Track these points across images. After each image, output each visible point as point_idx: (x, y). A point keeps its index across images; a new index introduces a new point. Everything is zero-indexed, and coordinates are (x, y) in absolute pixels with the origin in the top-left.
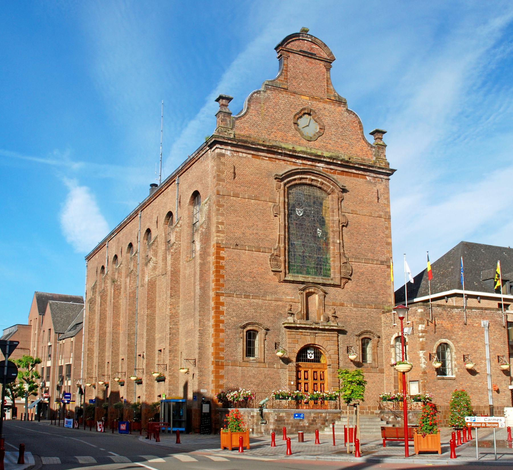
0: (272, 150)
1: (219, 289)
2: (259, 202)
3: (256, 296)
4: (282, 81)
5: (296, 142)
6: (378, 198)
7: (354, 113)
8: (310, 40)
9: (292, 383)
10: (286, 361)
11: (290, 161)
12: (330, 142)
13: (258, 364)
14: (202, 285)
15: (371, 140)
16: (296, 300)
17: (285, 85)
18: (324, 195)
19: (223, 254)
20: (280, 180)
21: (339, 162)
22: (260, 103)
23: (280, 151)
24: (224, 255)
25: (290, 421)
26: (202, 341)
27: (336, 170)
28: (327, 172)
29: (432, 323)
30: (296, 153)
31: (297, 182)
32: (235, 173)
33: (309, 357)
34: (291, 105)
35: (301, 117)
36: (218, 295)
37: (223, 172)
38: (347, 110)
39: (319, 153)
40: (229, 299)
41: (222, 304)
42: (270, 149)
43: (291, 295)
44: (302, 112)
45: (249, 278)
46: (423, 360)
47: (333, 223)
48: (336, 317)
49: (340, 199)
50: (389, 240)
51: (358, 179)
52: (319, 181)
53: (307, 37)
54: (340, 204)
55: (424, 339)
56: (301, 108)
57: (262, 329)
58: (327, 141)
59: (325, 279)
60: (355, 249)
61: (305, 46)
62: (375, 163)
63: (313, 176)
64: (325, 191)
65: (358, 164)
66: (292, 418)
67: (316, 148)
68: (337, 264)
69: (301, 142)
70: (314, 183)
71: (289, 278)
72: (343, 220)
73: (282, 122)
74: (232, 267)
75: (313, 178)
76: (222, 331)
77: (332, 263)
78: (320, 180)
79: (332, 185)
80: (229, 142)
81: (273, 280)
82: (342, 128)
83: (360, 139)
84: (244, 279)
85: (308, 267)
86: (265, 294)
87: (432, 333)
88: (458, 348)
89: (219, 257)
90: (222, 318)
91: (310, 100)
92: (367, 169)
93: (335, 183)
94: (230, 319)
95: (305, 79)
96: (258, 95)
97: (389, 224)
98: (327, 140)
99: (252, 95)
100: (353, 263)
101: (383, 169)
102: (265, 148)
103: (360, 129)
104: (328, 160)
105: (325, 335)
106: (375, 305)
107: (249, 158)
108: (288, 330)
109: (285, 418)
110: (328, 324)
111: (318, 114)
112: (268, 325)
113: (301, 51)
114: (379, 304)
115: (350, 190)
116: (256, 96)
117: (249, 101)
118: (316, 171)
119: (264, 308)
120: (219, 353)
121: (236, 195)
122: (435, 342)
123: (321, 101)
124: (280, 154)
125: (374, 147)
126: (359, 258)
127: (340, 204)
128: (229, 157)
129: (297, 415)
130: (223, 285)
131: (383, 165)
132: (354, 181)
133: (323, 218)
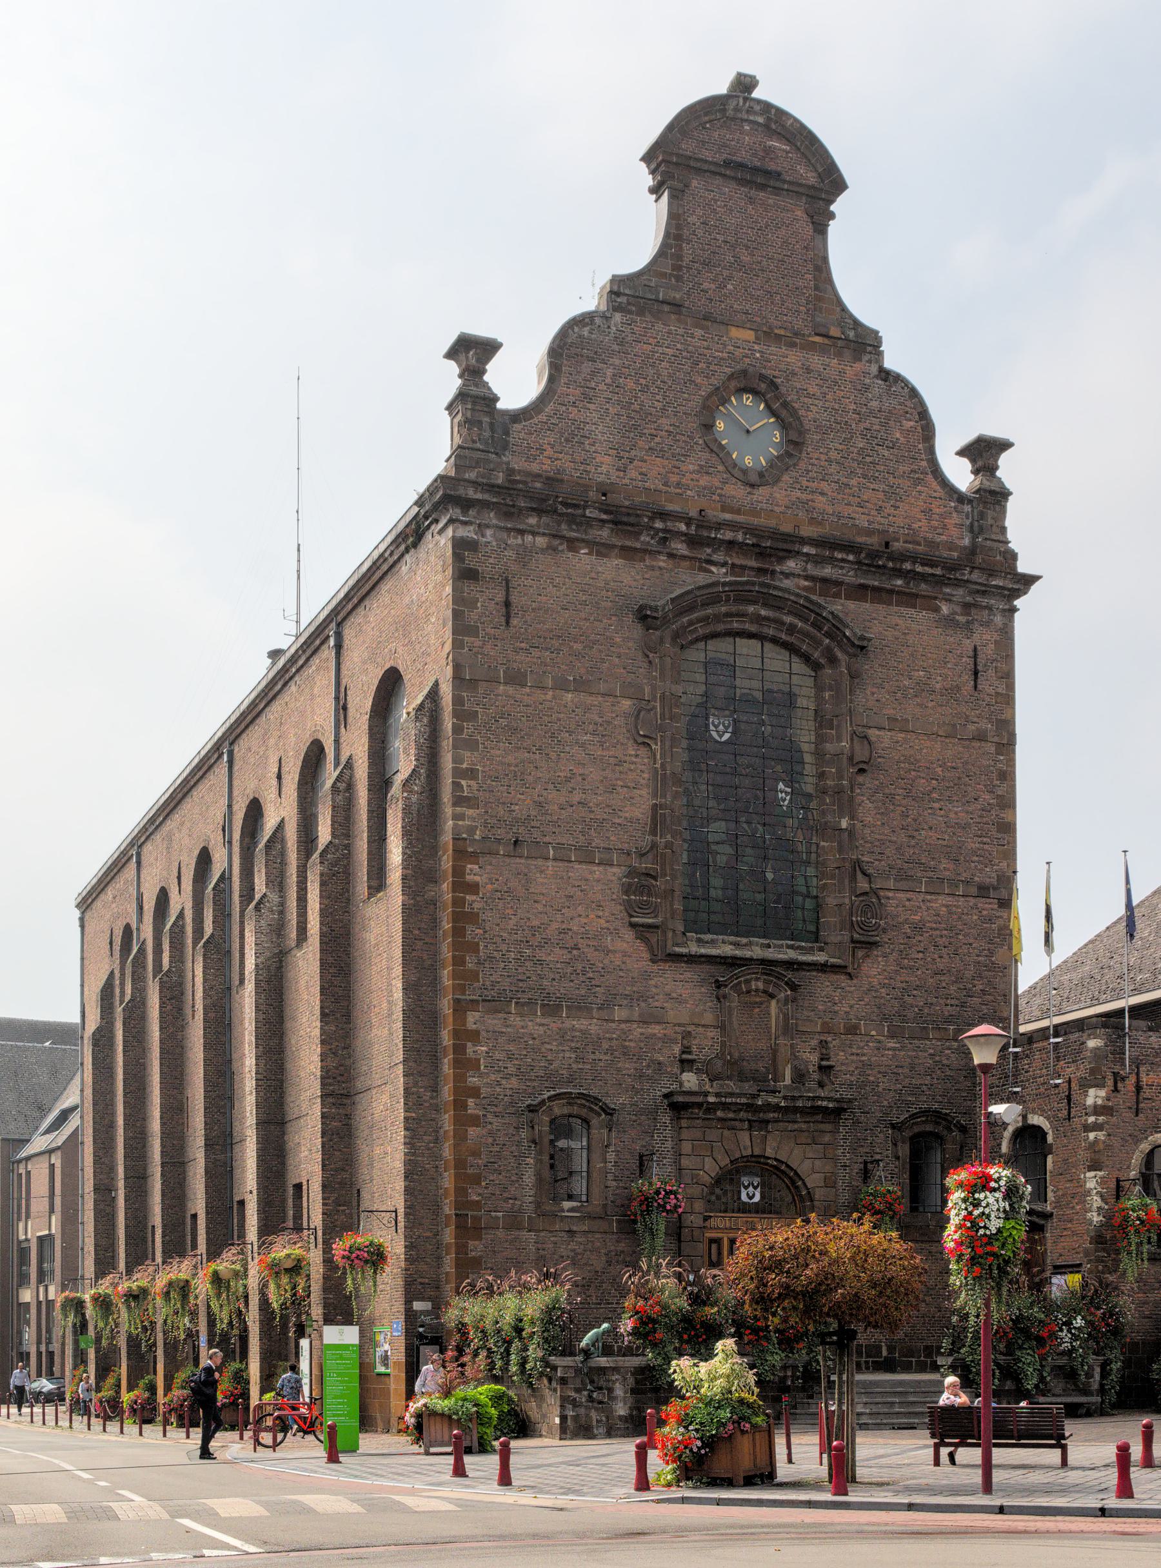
19: (473, 873)
36: (460, 1008)
41: (475, 1036)
46: (1097, 1202)
76: (475, 1121)
81: (628, 951)
86: (606, 1006)
89: (462, 886)
98: (813, 479)
119: (605, 1046)
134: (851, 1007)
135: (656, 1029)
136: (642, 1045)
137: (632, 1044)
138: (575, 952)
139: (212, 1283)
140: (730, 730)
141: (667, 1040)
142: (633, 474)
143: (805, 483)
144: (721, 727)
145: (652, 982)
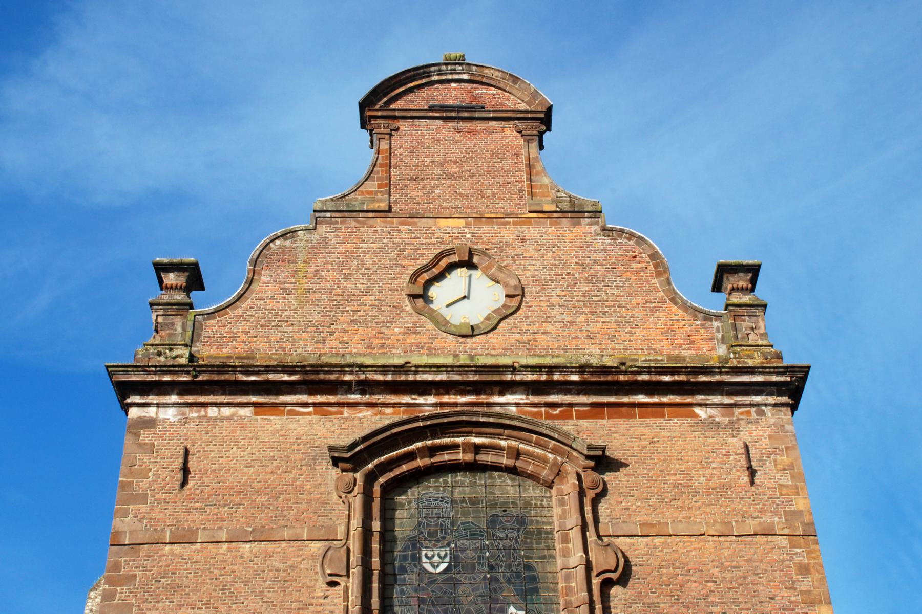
0: (318, 381)
2: (270, 547)
4: (371, 193)
5: (419, 346)
6: (752, 472)
8: (465, 77)
11: (394, 405)
12: (548, 327)
18: (533, 492)
20: (349, 466)
21: (575, 378)
22: (295, 262)
23: (348, 377)
27: (571, 405)
28: (539, 414)
30: (407, 373)
31: (420, 462)
32: (186, 470)
35: (440, 277)
44: (444, 263)
47: (567, 578)
49: (591, 494)
51: (660, 421)
53: (454, 72)
54: (588, 508)
58: (534, 328)
63: (479, 435)
67: (490, 351)
69: (437, 344)
70: (487, 458)
72: (602, 560)
73: (370, 300)
78: (503, 443)
79: (554, 451)
80: (166, 378)
82: (588, 281)
83: (663, 301)
92: (688, 383)
93: (564, 443)
95: (450, 176)
96: (288, 243)
101: (751, 370)
102: (294, 378)
103: (659, 274)
104: (530, 377)
113: (432, 108)
115: (632, 460)
116: (280, 247)
118: (485, 415)
121: (185, 538)
124: (348, 387)
125: (718, 317)
127: (588, 508)
128: (172, 424)
132: (646, 430)
133: (528, 567)
140: (447, 559)
142: (335, 344)
143: (525, 327)
144: (436, 559)
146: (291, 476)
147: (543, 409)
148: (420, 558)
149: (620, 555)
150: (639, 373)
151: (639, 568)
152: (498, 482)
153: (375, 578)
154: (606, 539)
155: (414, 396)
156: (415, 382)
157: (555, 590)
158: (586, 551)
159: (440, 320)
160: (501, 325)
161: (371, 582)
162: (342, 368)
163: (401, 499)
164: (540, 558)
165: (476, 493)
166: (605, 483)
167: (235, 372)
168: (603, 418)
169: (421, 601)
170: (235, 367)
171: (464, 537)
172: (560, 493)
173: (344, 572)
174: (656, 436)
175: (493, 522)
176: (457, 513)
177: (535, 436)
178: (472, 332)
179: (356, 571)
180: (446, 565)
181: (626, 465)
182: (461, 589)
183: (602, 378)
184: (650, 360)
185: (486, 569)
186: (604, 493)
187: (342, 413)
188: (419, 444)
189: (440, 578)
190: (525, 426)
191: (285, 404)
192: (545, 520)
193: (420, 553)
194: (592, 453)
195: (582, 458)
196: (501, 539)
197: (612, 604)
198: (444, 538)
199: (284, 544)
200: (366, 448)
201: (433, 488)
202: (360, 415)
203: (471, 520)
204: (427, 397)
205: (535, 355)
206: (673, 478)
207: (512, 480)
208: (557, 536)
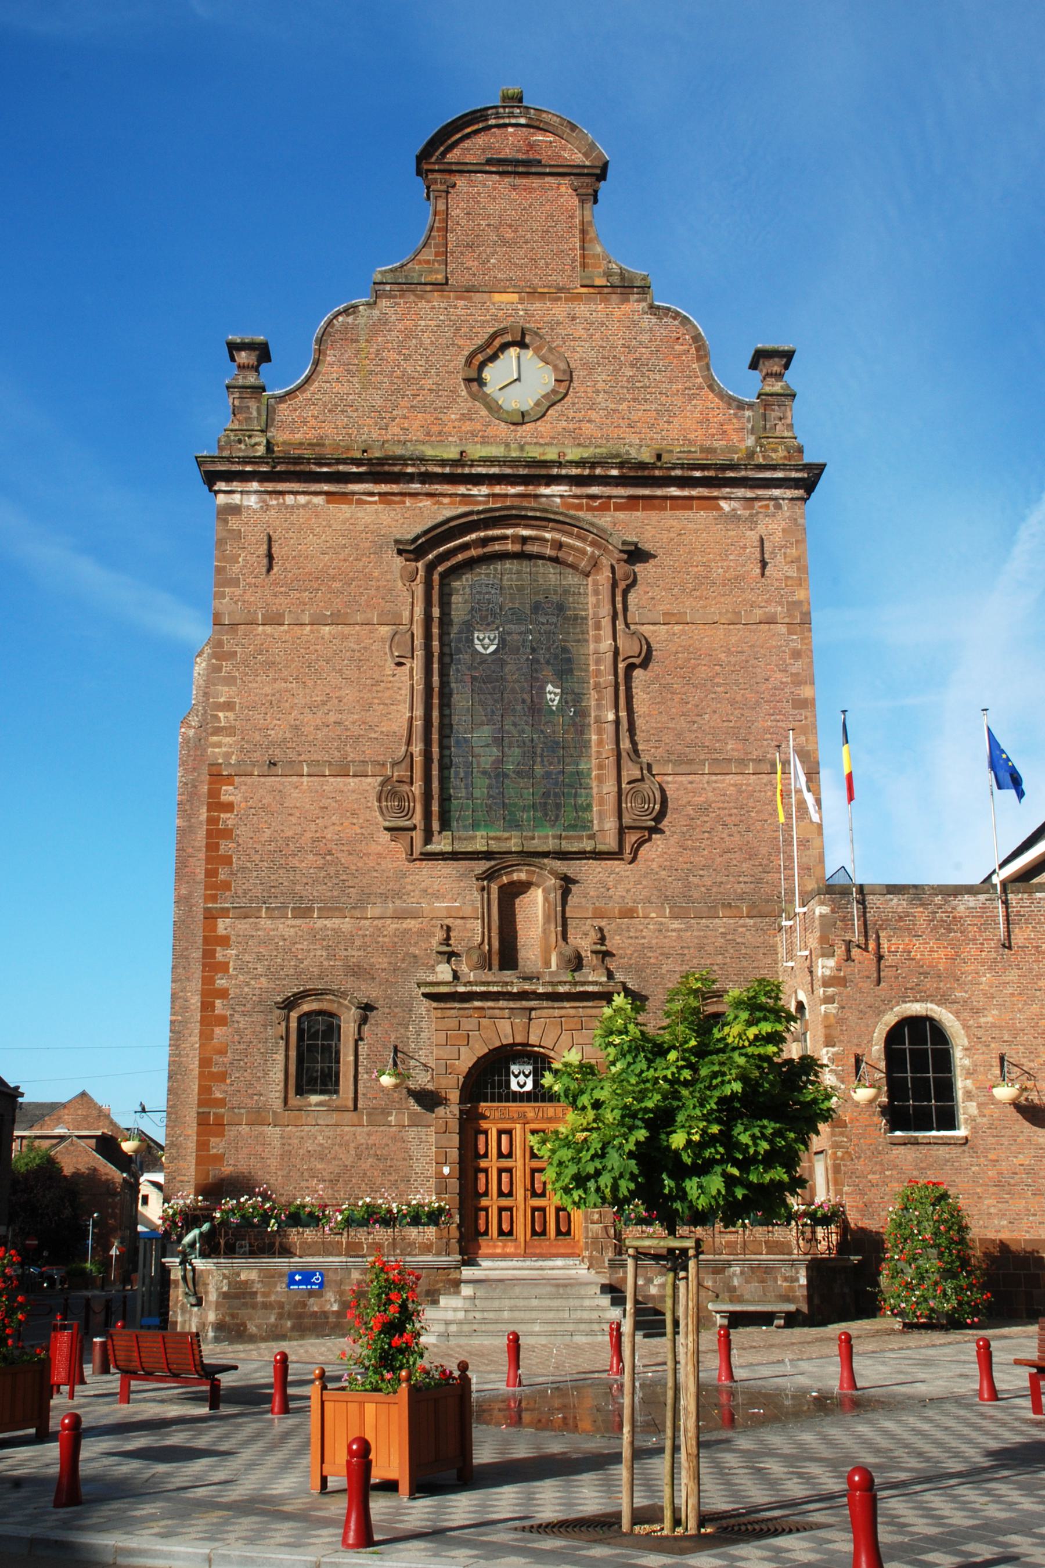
0: (384, 471)
1: (214, 898)
2: (347, 629)
3: (330, 908)
4: (428, 262)
6: (764, 564)
7: (678, 314)
8: (523, 121)
9: (446, 1170)
10: (429, 1100)
11: (451, 495)
12: (593, 415)
13: (335, 1115)
14: (184, 892)
15: (749, 385)
16: (468, 911)
17: (437, 272)
18: (572, 579)
19: (228, 793)
20: (412, 556)
21: (615, 472)
23: (410, 470)
24: (231, 798)
25: (273, 1298)
26: (179, 1055)
27: (610, 497)
29: (866, 950)
30: (463, 466)
31: (473, 552)
32: (270, 557)
33: (514, 1087)
34: (458, 329)
35: (493, 358)
37: (234, 559)
38: (651, 306)
39: (551, 455)
40: (243, 925)
41: (225, 941)
42: (379, 469)
43: (451, 896)
44: (497, 343)
45: (311, 857)
47: (598, 662)
48: (607, 954)
49: (622, 585)
50: (806, 692)
52: (547, 541)
55: (832, 1008)
56: (491, 331)
57: (350, 1009)
58: (580, 416)
59: (566, 838)
60: (679, 735)
61: (508, 142)
62: (751, 454)
63: (527, 527)
64: (573, 567)
65: (682, 466)
66: (281, 1287)
67: (541, 443)
68: (610, 787)
69: (490, 432)
70: (533, 548)
71: (441, 844)
72: (628, 647)
73: (428, 383)
74: (258, 831)
75: (526, 532)
76: (222, 1021)
77: (594, 784)
78: (548, 536)
79: (593, 544)
80: (248, 468)
81: (387, 852)
82: (632, 366)
84: (295, 862)
85: (515, 805)
86: (360, 904)
87: (868, 985)
88: (980, 1033)
90: (221, 982)
91: (521, 301)
92: (716, 478)
93: (601, 539)
94: (248, 984)
95: (505, 243)
96: (350, 319)
97: (806, 640)
98: (579, 410)
99: (330, 323)
100: (670, 778)
101: (774, 468)
103: (699, 358)
104: (574, 471)
105: (563, 1012)
106: (753, 906)
107: (316, 506)
108: (435, 1005)
109: (257, 1287)
110: (578, 976)
111: (548, 338)
112: (367, 991)
113: (489, 162)
114: (767, 901)
115: (660, 552)
116: (345, 325)
117: (320, 341)
118: (533, 509)
119: (358, 943)
120: (210, 1088)
122: (880, 1013)
123: (560, 298)
124: (411, 478)
126: (691, 762)
127: (619, 599)
128: (255, 511)
129: (297, 1278)
130: (226, 886)
131: (778, 456)
132: (675, 523)
133: (565, 650)
134: (628, 891)
135: (411, 924)
136: (396, 940)
137: (386, 940)
138: (328, 858)
139: (367, 1004)
140: (496, 642)
141: (421, 933)
142: (397, 430)
143: (571, 415)
144: (487, 641)
145: (408, 880)
146: (361, 564)
147: (584, 501)
148: (473, 640)
149: (644, 642)
150: (673, 468)
151: (659, 653)
152: (541, 570)
153: (436, 659)
154: (632, 627)
155: (469, 487)
156: (471, 475)
157: (587, 671)
158: (615, 639)
159: (493, 405)
160: (550, 412)
161: (432, 663)
162: (403, 460)
163: (456, 584)
164: (575, 641)
165: (523, 580)
166: (635, 574)
167: (309, 463)
168: (638, 510)
169: (474, 679)
170: (309, 459)
171: (511, 622)
172: (596, 583)
173: (409, 655)
174: (683, 528)
175: (536, 608)
176: (505, 599)
177: (576, 529)
178: (522, 419)
179: (419, 653)
180: (495, 647)
181: (655, 557)
182: (507, 669)
183: (640, 474)
184: (684, 452)
185: (529, 651)
186: (634, 583)
187: (404, 503)
188: (474, 536)
189: (490, 659)
190: (567, 520)
191: (354, 493)
192: (581, 606)
193: (473, 635)
194: (625, 548)
195: (617, 552)
196: (543, 624)
197: (634, 685)
198: (493, 622)
199: (357, 627)
200: (426, 541)
201: (483, 574)
202: (420, 505)
203: (517, 606)
204: (480, 487)
205: (579, 445)
206: (696, 569)
207: (554, 568)
208: (591, 622)
